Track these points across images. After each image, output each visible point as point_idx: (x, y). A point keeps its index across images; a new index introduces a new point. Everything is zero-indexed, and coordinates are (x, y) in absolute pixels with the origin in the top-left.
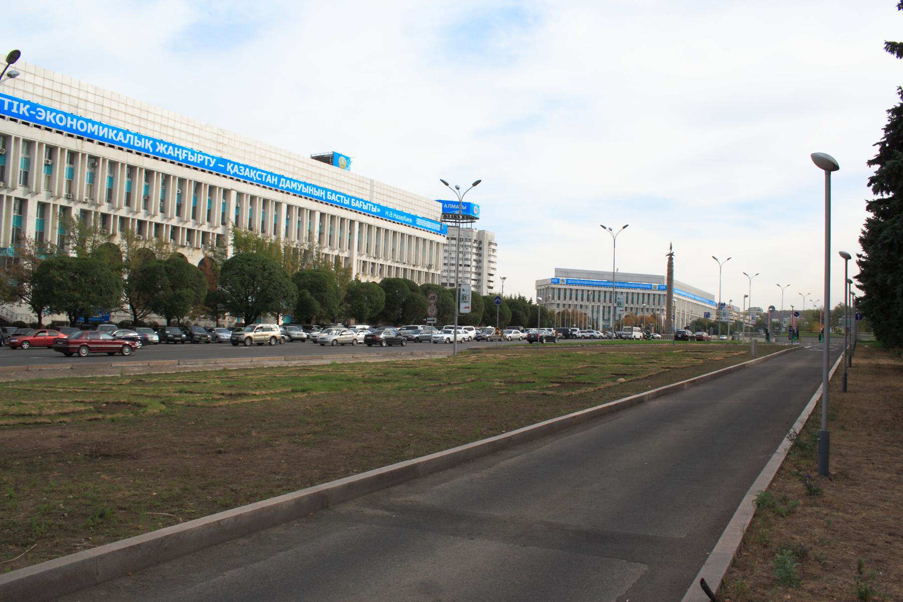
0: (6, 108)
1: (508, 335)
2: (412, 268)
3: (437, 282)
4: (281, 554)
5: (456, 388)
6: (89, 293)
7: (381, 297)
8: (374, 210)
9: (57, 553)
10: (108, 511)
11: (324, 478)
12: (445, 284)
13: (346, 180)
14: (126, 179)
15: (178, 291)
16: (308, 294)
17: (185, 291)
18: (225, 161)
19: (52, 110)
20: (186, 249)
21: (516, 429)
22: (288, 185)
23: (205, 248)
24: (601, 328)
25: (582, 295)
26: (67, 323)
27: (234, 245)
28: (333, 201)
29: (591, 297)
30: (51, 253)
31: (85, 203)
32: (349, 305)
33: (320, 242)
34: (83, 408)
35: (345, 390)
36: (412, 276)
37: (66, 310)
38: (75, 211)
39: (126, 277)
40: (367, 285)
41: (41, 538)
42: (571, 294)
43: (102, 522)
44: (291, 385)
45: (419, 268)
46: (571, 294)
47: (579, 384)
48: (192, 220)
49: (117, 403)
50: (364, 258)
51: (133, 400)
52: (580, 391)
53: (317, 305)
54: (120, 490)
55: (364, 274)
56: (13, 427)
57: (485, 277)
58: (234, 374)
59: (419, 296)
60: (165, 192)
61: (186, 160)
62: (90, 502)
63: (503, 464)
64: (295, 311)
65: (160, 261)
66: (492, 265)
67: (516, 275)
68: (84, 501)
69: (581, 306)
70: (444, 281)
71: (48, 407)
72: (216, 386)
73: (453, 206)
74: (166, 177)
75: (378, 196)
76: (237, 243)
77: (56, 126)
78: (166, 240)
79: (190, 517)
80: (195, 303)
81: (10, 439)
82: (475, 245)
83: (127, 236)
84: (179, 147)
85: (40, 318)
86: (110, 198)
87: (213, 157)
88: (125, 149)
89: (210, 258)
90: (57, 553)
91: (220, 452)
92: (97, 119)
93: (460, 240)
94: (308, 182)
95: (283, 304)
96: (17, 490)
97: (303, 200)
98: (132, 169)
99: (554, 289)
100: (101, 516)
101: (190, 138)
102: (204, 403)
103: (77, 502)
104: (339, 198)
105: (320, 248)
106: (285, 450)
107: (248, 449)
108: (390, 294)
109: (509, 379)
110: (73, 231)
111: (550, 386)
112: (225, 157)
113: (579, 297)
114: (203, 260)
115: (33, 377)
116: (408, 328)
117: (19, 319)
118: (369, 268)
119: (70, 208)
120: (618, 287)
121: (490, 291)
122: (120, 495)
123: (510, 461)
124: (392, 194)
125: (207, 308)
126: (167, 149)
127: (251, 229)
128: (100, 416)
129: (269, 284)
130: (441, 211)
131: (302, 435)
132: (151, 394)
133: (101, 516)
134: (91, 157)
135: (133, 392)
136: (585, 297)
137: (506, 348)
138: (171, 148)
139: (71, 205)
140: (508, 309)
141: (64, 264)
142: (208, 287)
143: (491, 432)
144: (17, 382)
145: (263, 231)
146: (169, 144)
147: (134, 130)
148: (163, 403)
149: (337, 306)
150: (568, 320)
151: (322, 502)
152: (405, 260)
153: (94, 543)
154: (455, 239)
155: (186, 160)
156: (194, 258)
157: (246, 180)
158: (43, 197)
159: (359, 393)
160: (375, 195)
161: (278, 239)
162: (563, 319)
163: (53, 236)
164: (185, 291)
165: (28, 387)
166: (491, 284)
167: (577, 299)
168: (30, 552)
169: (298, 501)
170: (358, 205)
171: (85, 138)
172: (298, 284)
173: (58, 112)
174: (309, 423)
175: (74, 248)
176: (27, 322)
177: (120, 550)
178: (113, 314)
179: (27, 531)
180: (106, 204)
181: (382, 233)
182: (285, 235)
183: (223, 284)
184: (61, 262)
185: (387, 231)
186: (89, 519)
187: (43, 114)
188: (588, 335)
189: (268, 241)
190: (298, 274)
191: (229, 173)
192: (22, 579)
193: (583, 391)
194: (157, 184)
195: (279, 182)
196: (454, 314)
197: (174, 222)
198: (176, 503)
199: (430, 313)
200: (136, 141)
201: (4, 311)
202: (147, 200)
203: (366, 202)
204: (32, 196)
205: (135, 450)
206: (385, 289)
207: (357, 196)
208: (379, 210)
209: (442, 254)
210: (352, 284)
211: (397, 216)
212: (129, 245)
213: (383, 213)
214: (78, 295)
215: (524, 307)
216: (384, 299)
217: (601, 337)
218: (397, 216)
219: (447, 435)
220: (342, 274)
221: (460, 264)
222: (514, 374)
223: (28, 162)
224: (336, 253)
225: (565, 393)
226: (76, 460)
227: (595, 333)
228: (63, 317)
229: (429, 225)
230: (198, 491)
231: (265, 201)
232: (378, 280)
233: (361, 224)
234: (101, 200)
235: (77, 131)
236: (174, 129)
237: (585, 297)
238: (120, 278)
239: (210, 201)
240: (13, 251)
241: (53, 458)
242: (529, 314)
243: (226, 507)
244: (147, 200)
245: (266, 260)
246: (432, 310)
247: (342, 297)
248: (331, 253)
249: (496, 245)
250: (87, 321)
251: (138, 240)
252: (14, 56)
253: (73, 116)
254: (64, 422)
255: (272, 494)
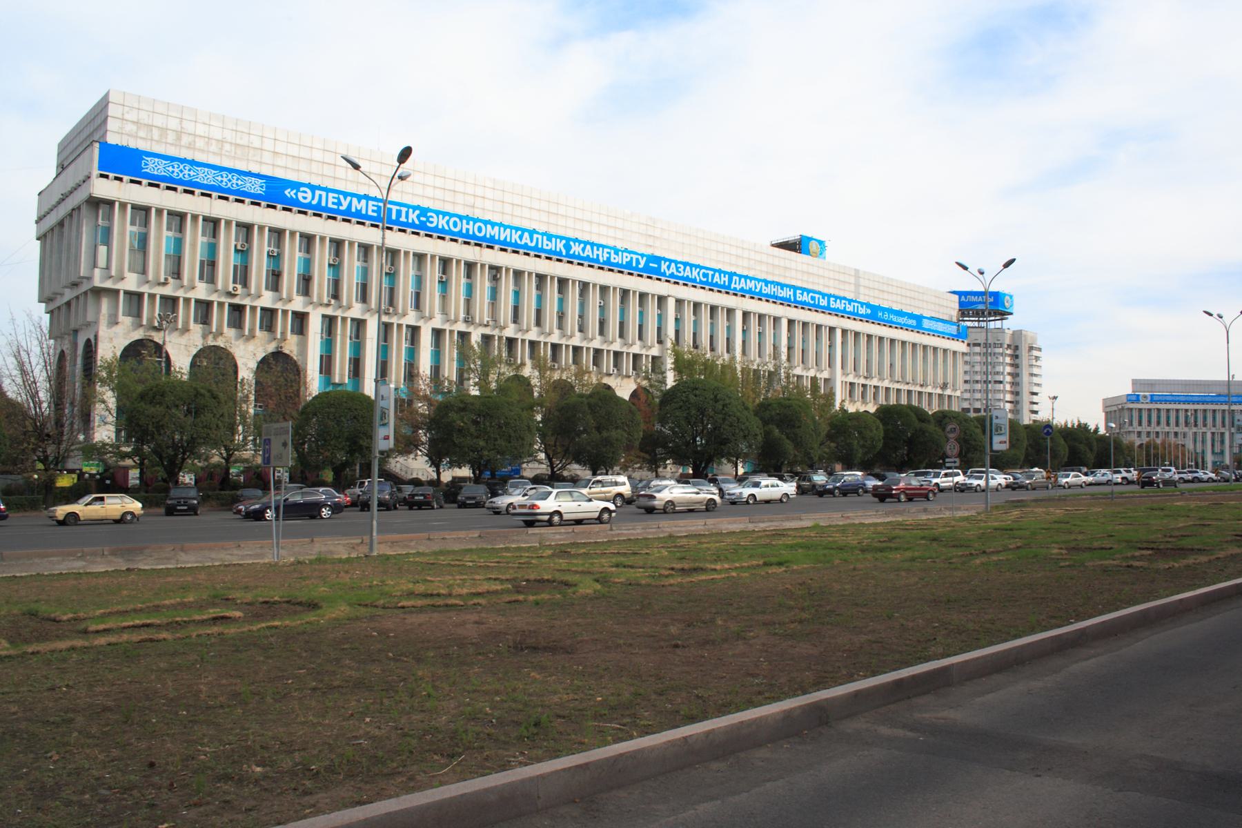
0: (394, 217)
1: (1065, 480)
2: (918, 389)
3: (955, 408)
4: (768, 785)
5: (995, 558)
6: (496, 440)
7: (878, 432)
8: (862, 311)
9: (489, 768)
10: (544, 718)
11: (820, 684)
12: (968, 410)
13: (821, 272)
14: (534, 291)
15: (605, 434)
16: (776, 432)
17: (614, 434)
18: (658, 260)
19: (445, 214)
20: (612, 378)
21: (1090, 617)
22: (743, 285)
23: (638, 375)
24: (1210, 465)
25: (1177, 417)
26: (470, 478)
27: (674, 369)
28: (805, 303)
29: (1192, 420)
30: (450, 392)
31: (486, 326)
32: (833, 445)
33: (789, 360)
34: (499, 588)
35: (837, 562)
36: (920, 402)
37: (469, 462)
38: (475, 338)
39: (539, 418)
40: (857, 416)
41: (468, 748)
42: (1159, 417)
43: (538, 735)
44: (762, 556)
45: (929, 389)
46: (1159, 417)
47: (1183, 551)
48: (618, 340)
49: (539, 581)
50: (851, 379)
51: (559, 576)
52: (1185, 562)
53: (789, 446)
54: (555, 693)
55: (852, 401)
56: (421, 610)
57: (1026, 397)
58: (684, 542)
59: (932, 427)
60: (583, 305)
61: (608, 262)
62: (521, 707)
63: (1075, 668)
64: (760, 455)
65: (581, 396)
66: (1035, 380)
67: (1071, 394)
68: (514, 705)
69: (1176, 434)
70: (966, 405)
71: (458, 585)
72: (662, 558)
73: (974, 299)
74: (584, 286)
75: (867, 292)
76: (680, 366)
77: (450, 232)
78: (588, 367)
79: (646, 731)
80: (628, 448)
81: (420, 625)
82: (1009, 352)
83: (539, 365)
84: (599, 246)
85: (439, 474)
86: (516, 318)
87: (643, 256)
88: (532, 253)
89: (645, 389)
90: (489, 768)
91: (676, 646)
92: (496, 218)
93: (986, 345)
94: (770, 278)
95: (743, 447)
96: (435, 687)
97: (763, 303)
98: (541, 278)
99: (1131, 409)
100: (536, 725)
101: (611, 233)
102: (649, 580)
103: (506, 705)
104: (813, 298)
105: (791, 368)
106: (764, 645)
107: (713, 642)
108: (890, 427)
109: (1073, 544)
110: (474, 363)
111: (1137, 553)
112: (658, 254)
113: (1172, 420)
114: (635, 391)
115: (436, 548)
116: (917, 475)
117: (414, 476)
118: (858, 391)
119: (307, 314)
120: (1235, 403)
121: (1034, 417)
122: (556, 699)
123: (1084, 664)
124: (885, 288)
125: (642, 454)
126: (583, 250)
127: (695, 346)
128: (521, 597)
129: (724, 419)
130: (957, 306)
131: (784, 624)
132: (580, 569)
133: (536, 725)
134: (492, 267)
135: (557, 567)
136: (1182, 420)
137: (1062, 500)
138: (588, 247)
139: (471, 329)
140: (1062, 442)
141: (464, 404)
142: (643, 426)
143: (1053, 621)
144: (418, 554)
145: (712, 349)
146: (586, 243)
147: (542, 228)
148: (597, 581)
149: (816, 446)
150: (1156, 456)
151: (820, 716)
152: (909, 378)
153: (531, 759)
154: (979, 345)
155: (608, 262)
156: (624, 389)
157: (687, 282)
158: (437, 323)
159: (859, 565)
160: (862, 290)
161: (733, 358)
162: (1148, 455)
163: (450, 370)
164: (614, 434)
165: (432, 560)
166: (1035, 407)
167: (1168, 424)
168: (458, 764)
169: (788, 715)
170: (839, 305)
171: (484, 244)
172: (761, 419)
173: (452, 215)
174: (791, 608)
175: (476, 384)
176: (424, 478)
177: (564, 770)
178: (524, 465)
179: (451, 738)
180: (512, 326)
181: (875, 343)
182: (741, 353)
183: (663, 421)
184: (462, 401)
185: (881, 339)
186: (522, 729)
187: (435, 220)
188: (1190, 477)
189: (720, 362)
190: (761, 405)
191: (664, 274)
192: (455, 797)
193: (1190, 560)
194: (573, 294)
195: (730, 281)
196: (983, 452)
197: (597, 343)
198: (627, 712)
199: (949, 453)
200: (545, 242)
201: (398, 465)
202: (561, 316)
203: (850, 301)
204: (314, 309)
205: (568, 642)
206: (881, 420)
207: (837, 293)
208: (869, 311)
209: (961, 368)
210: (835, 415)
211: (894, 318)
212: (542, 376)
213: (875, 314)
214: (482, 443)
215: (1087, 439)
216: (882, 434)
217: (1210, 480)
218: (894, 318)
219: (988, 625)
220: (822, 401)
221: (989, 380)
222: (1080, 537)
223: (419, 281)
224: (812, 373)
225: (1162, 565)
226: (498, 652)
227: (1200, 474)
228: (465, 472)
229: (940, 327)
230: (654, 697)
231: (713, 309)
232: (872, 409)
233: (844, 332)
234: (528, 325)
235: (474, 237)
236: (591, 222)
237: (1182, 420)
238: (532, 418)
239: (641, 313)
240: (406, 390)
241: (471, 650)
242: (1095, 448)
243: (692, 719)
244: (561, 316)
245: (717, 388)
246: (952, 448)
247: (824, 434)
248: (804, 374)
249: (1040, 350)
250: (493, 476)
251: (552, 369)
252: (405, 154)
253: (468, 218)
254: (479, 604)
255: (751, 704)
